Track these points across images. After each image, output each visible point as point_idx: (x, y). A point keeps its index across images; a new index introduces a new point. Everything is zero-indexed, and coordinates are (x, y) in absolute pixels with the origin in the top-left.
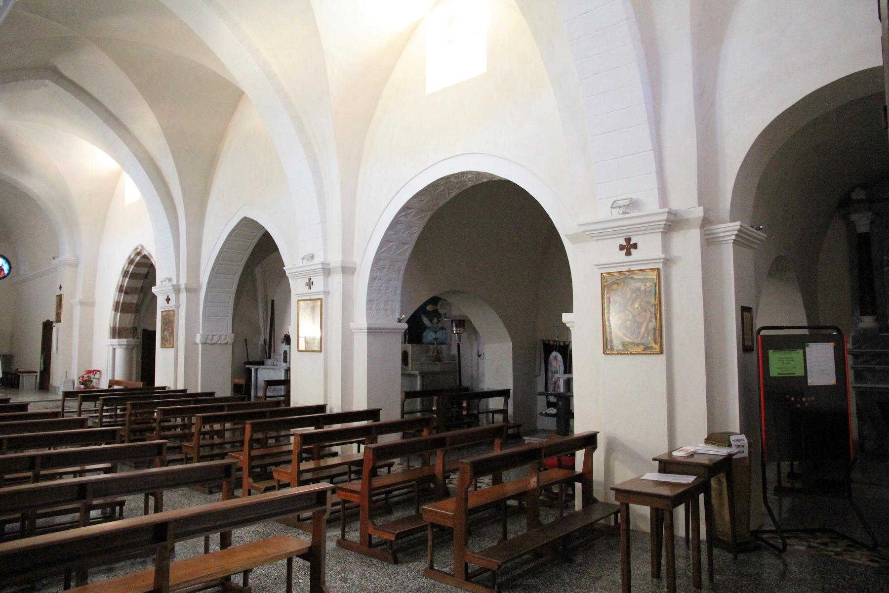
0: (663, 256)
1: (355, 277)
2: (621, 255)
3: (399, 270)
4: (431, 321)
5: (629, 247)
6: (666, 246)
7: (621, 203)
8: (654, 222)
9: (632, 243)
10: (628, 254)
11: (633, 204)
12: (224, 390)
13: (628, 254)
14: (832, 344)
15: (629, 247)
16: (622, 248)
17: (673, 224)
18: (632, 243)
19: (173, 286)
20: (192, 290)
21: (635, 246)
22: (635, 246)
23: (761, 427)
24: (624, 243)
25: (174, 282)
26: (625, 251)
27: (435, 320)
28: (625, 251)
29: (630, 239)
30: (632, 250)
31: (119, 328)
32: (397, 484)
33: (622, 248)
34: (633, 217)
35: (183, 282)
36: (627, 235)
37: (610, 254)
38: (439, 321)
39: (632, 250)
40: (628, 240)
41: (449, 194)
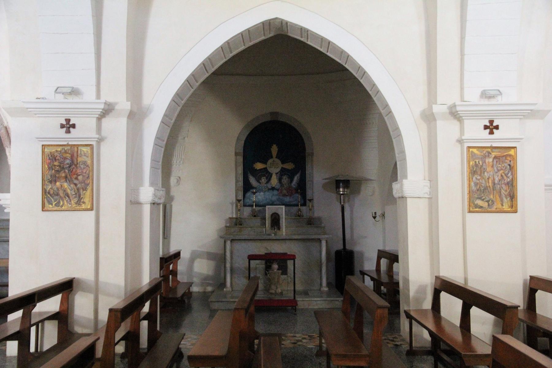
0: (97, 136)
4: (258, 181)
6: (99, 129)
7: (65, 90)
8: (526, 110)
9: (71, 123)
11: (74, 92)
15: (491, 128)
17: (108, 110)
18: (71, 123)
21: (74, 126)
22: (497, 127)
23: (316, 301)
24: (64, 123)
26: (65, 129)
27: (263, 180)
29: (69, 120)
30: (71, 129)
34: (76, 103)
36: (491, 118)
38: (267, 183)
41: (213, 67)
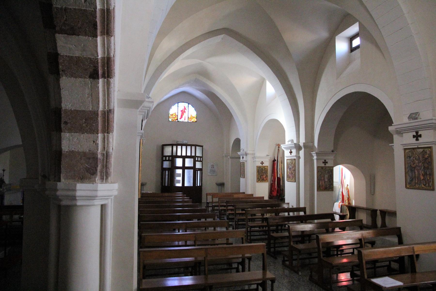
1: (110, 135)
2: (414, 141)
3: (72, 136)
5: (417, 136)
10: (417, 140)
12: (170, 167)
13: (417, 140)
14: (349, 273)
16: (414, 136)
19: (295, 144)
20: (308, 147)
21: (420, 136)
22: (420, 136)
25: (295, 142)
26: (415, 138)
28: (415, 138)
31: (98, 78)
32: (83, 199)
33: (414, 136)
35: (302, 141)
37: (408, 139)
39: (419, 138)
40: (417, 133)
